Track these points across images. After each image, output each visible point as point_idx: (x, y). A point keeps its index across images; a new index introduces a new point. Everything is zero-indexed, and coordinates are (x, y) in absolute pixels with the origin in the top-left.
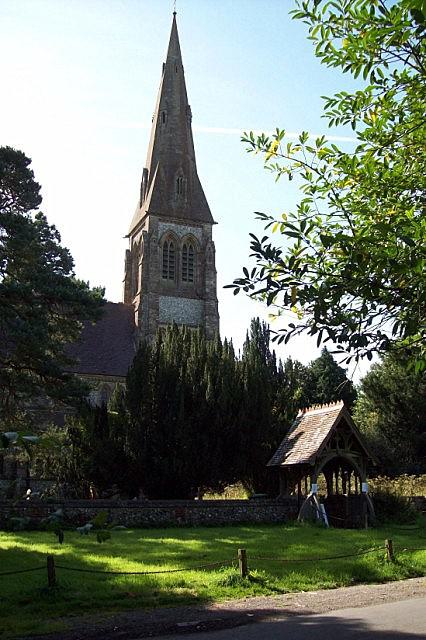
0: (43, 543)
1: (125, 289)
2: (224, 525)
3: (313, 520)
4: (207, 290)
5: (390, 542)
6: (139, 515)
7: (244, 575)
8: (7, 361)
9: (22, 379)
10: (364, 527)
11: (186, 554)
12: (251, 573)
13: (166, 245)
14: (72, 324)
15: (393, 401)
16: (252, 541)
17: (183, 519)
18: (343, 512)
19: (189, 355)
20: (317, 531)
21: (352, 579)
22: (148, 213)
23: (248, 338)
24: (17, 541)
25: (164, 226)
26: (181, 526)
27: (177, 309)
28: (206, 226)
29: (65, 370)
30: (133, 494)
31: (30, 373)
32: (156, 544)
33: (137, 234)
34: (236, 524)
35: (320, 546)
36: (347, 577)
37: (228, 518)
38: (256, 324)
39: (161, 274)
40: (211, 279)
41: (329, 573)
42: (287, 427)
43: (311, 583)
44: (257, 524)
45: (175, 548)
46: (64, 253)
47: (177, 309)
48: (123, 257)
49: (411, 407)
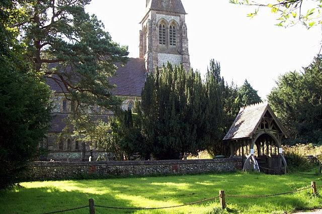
0: (30, 189)
1: (140, 51)
2: (200, 174)
3: (251, 170)
4: (183, 50)
5: (314, 183)
6: (151, 169)
7: (224, 208)
8: (75, 87)
9: (84, 96)
10: (284, 174)
11: (179, 193)
12: (228, 206)
13: (160, 26)
14: (111, 66)
15: (285, 105)
16: (218, 183)
17: (176, 171)
18: (267, 165)
19: (176, 79)
20: (256, 176)
21: (294, 209)
22: (150, 10)
23: (208, 71)
24: (78, 186)
25: (159, 16)
26: (175, 175)
27: (167, 59)
28: (182, 16)
29: (109, 91)
30: (147, 158)
31: (89, 94)
32: (162, 186)
33: (144, 21)
34: (207, 173)
35: (261, 186)
36: (290, 207)
37: (201, 170)
38: (213, 63)
39: (159, 42)
40: (185, 43)
41: (278, 205)
42: (232, 120)
43: (268, 212)
44: (219, 173)
45: (174, 189)
46: (106, 34)
47: (167, 59)
48: (138, 35)
49: (296, 108)
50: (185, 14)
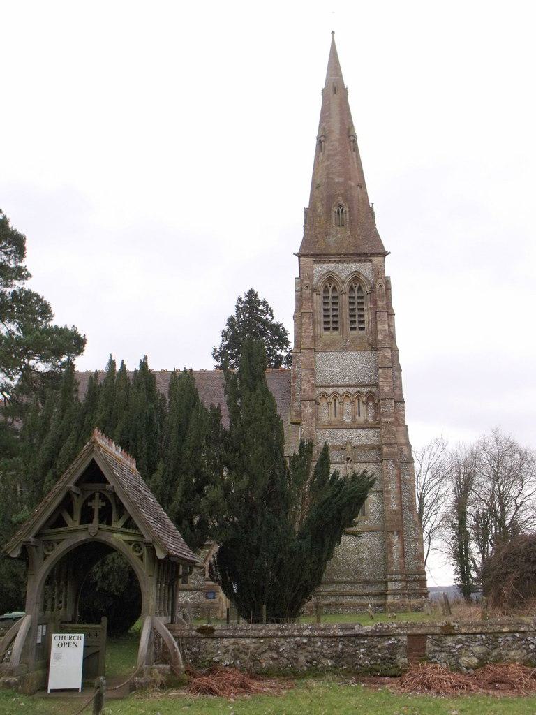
13: (326, 290)
25: (321, 269)
28: (376, 260)
40: (383, 322)
50: (384, 254)
